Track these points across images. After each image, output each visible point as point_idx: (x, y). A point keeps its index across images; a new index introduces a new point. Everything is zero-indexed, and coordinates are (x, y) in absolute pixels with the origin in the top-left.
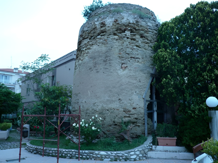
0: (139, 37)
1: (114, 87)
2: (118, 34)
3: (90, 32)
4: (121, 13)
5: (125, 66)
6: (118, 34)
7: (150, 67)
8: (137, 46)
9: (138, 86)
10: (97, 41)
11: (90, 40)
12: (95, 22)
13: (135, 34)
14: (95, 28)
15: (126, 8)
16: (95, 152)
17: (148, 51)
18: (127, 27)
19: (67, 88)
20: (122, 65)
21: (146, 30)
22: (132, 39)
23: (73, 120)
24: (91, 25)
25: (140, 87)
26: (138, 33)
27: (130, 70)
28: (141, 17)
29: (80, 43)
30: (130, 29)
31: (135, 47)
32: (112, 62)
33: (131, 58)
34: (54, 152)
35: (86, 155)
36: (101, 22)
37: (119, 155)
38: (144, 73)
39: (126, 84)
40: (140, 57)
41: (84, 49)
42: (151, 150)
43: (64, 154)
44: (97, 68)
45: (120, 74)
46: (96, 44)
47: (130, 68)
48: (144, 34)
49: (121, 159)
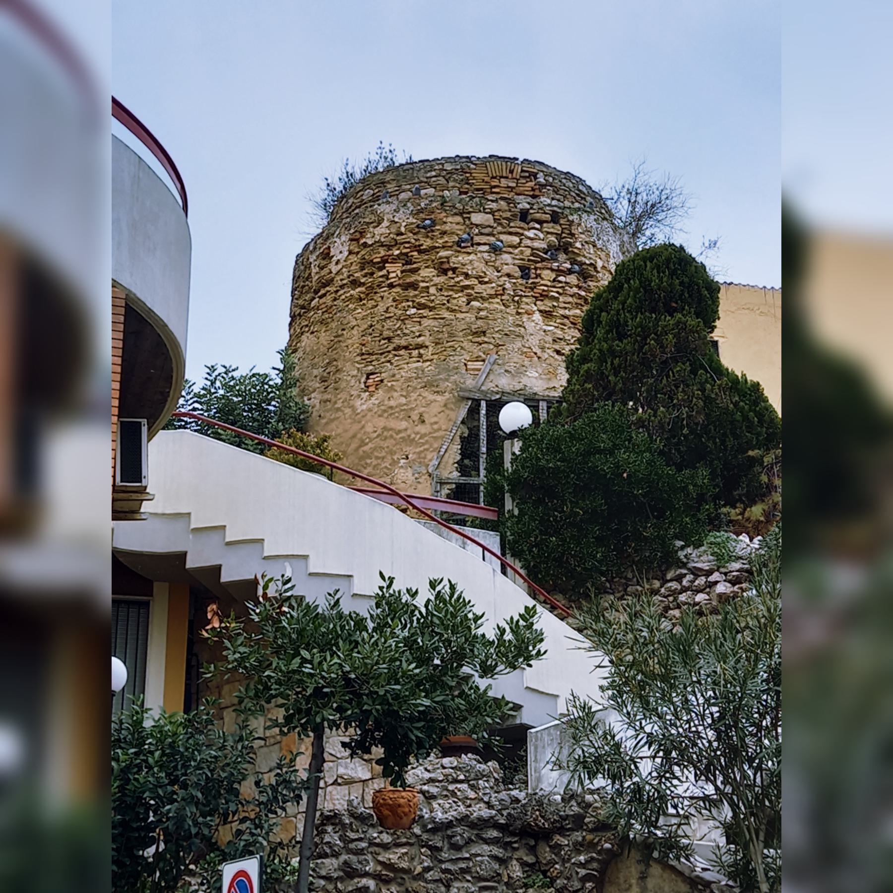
9: (413, 436)
20: (368, 378)
31: (413, 311)
39: (377, 437)
40: (426, 340)
47: (389, 384)
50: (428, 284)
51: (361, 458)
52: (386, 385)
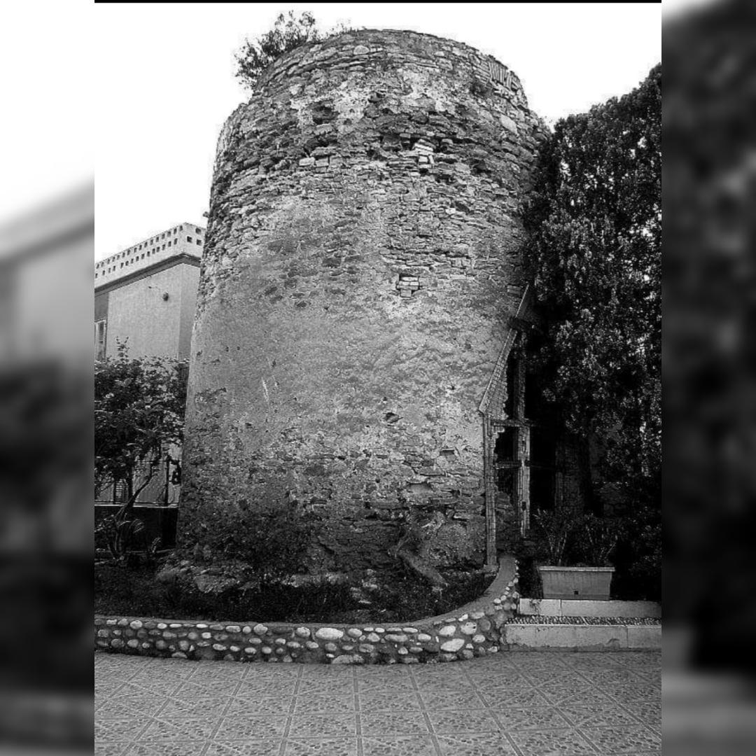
0: (469, 172)
1: (368, 367)
2: (385, 154)
3: (270, 140)
4: (400, 70)
5: (412, 284)
6: (385, 154)
7: (509, 294)
8: (461, 207)
10: (298, 179)
11: (266, 173)
12: (292, 100)
13: (452, 156)
14: (291, 123)
15: (417, 52)
16: (296, 629)
17: (499, 229)
18: (423, 129)
19: (159, 370)
20: (400, 280)
21: (493, 143)
22: (439, 177)
23: (190, 499)
24: (275, 112)
25: (468, 368)
26: (462, 154)
27: (432, 300)
28: (477, 90)
29: (222, 184)
30: (435, 136)
31: (453, 211)
32: (360, 266)
33: (438, 251)
34: (116, 632)
35: (258, 641)
36: (318, 99)
37: (394, 637)
38: (485, 316)
39: (418, 355)
41: (243, 211)
42: (516, 615)
43: (164, 639)
44: (297, 291)
45: (390, 317)
46: (294, 190)
47: (430, 294)
48: (486, 160)
49: (401, 655)
50: (465, 183)
51: (398, 378)
52: (425, 294)
